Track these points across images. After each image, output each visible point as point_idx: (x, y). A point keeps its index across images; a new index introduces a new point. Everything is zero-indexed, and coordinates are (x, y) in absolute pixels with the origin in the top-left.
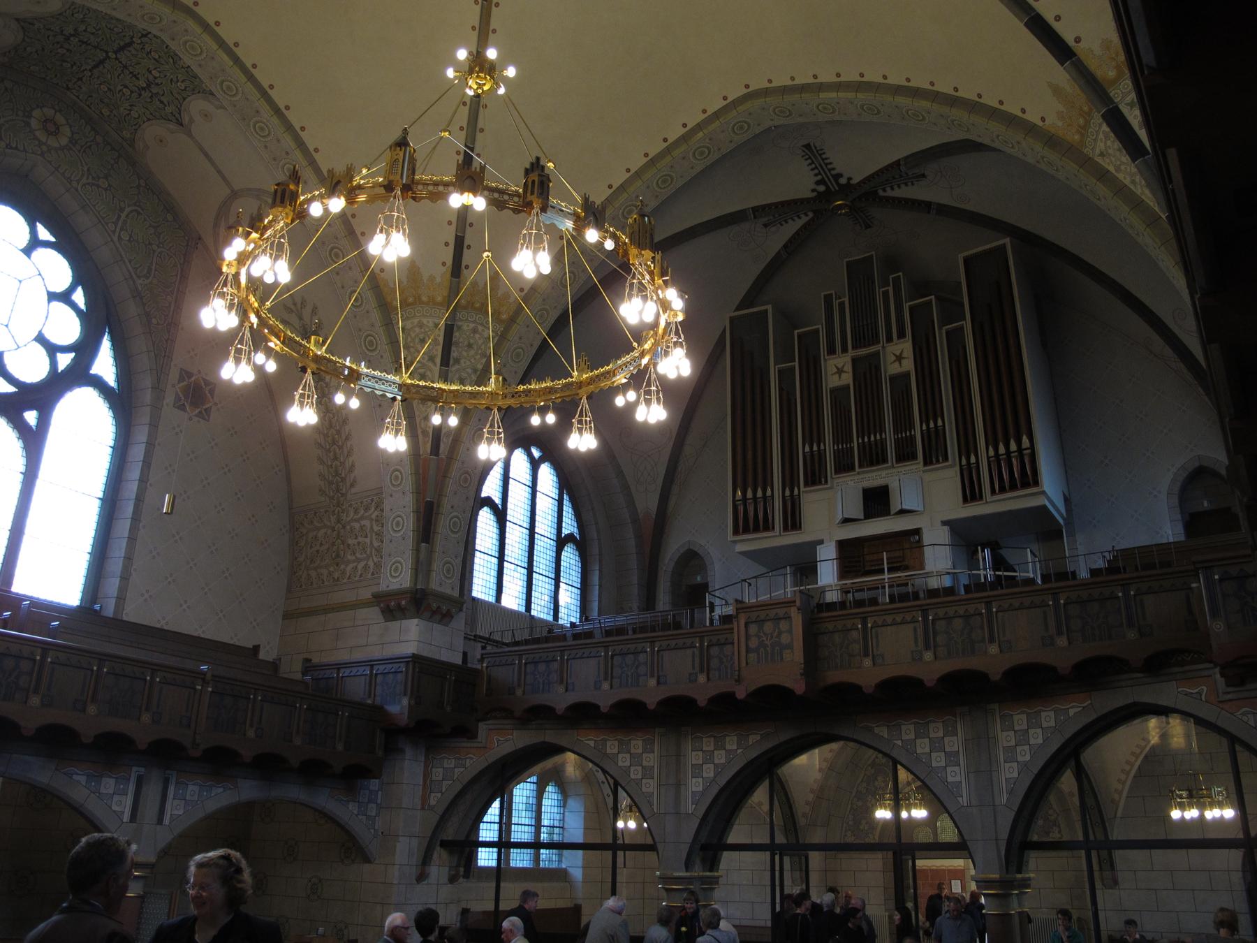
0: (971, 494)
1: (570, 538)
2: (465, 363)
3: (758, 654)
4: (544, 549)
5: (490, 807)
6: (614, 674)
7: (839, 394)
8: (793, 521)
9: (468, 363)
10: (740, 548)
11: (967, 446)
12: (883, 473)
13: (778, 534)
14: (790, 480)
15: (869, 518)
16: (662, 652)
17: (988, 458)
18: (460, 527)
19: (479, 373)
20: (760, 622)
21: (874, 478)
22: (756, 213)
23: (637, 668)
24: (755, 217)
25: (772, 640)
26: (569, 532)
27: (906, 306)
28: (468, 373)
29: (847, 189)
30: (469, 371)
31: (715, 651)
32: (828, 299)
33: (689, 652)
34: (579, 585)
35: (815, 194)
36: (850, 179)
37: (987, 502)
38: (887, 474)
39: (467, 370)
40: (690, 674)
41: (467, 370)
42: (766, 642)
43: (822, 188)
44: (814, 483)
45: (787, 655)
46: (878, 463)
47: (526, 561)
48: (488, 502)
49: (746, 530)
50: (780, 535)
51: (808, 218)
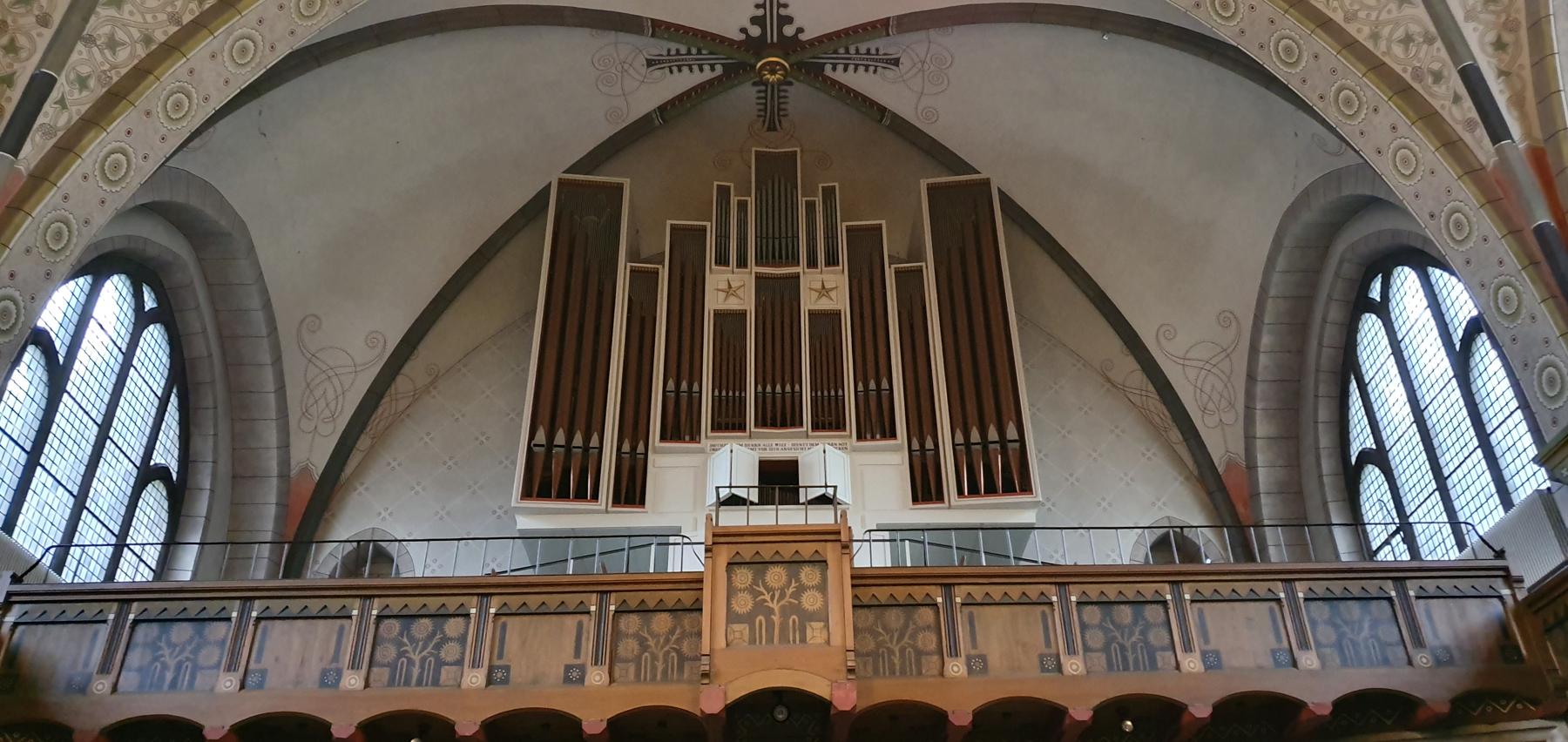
0: (925, 488)
1: (162, 473)
2: (131, 13)
3: (752, 629)
4: (116, 475)
5: (1362, 515)
6: (378, 656)
7: (730, 322)
8: (631, 491)
9: (138, 18)
10: (525, 523)
11: (921, 422)
12: (789, 443)
13: (603, 507)
14: (633, 427)
15: (763, 505)
16: (504, 619)
17: (954, 445)
18: (15, 324)
19: (154, 47)
20: (760, 565)
21: (779, 446)
22: (657, 29)
23: (438, 647)
24: (653, 36)
25: (782, 602)
26: (163, 462)
27: (842, 227)
28: (130, 36)
29: (790, 46)
30: (137, 35)
31: (631, 623)
32: (724, 192)
33: (570, 622)
34: (155, 563)
35: (742, 37)
36: (800, 30)
37: (950, 507)
38: (793, 445)
39: (132, 30)
40: (568, 668)
41: (132, 30)
42: (770, 605)
43: (755, 31)
44: (677, 437)
45: (815, 632)
46: (784, 425)
47: (79, 483)
48: (41, 339)
49: (544, 494)
50: (607, 512)
51: (713, 75)
